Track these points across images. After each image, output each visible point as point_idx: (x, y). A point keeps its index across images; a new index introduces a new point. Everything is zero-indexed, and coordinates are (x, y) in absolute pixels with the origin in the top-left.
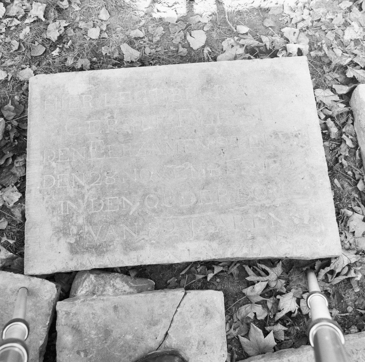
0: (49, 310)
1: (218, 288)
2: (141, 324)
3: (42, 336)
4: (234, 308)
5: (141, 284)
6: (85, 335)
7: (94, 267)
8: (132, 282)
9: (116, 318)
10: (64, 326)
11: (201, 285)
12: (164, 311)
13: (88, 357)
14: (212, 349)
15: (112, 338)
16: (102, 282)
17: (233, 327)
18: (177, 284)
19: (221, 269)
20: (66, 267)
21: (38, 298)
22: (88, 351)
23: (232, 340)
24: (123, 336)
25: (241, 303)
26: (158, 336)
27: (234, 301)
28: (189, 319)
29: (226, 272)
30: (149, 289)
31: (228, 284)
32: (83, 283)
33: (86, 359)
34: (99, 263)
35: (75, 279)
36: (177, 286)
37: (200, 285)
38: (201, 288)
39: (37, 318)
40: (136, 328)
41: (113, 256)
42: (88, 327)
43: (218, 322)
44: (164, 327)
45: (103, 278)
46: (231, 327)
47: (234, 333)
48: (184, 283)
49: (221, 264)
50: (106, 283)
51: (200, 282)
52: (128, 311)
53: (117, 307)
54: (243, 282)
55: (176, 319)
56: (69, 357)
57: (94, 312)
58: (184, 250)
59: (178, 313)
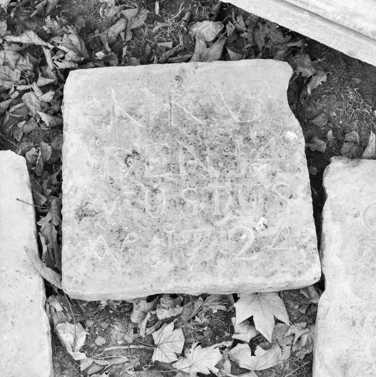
4: (287, 368)
43: (329, 350)
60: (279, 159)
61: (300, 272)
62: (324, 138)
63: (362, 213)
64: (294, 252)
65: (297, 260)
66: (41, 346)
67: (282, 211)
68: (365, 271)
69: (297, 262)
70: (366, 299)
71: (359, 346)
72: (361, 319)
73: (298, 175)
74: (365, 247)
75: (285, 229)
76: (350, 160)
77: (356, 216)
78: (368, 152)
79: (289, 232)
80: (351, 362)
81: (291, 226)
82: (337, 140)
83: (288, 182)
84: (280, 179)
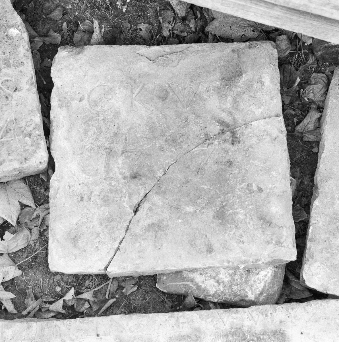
0: (310, 247)
1: (59, 277)
2: (172, 226)
3: (317, 212)
4: (37, 247)
5: (176, 285)
6: (253, 213)
7: (246, 310)
8: (190, 288)
9: (209, 236)
10: (283, 225)
11: (85, 282)
12: (138, 244)
13: (246, 184)
14: (71, 190)
15: (214, 208)
16: (235, 288)
17: (40, 220)
18: (123, 284)
19: (52, 307)
20: (290, 310)
21: (329, 264)
22: (247, 191)
23: (44, 202)
24: (198, 211)
25: (26, 254)
26: (148, 210)
27: (36, 257)
28: (103, 232)
29: (45, 302)
30: (165, 278)
31: (43, 283)
32: (265, 286)
33: (250, 181)
34: (238, 315)
35: (279, 292)
36: (122, 281)
37: (87, 282)
38: (86, 277)
39: (327, 236)
40: (180, 221)
41: (217, 328)
42: (249, 223)
43: (61, 226)
44: (139, 221)
45: (234, 294)
46: (43, 219)
47: (39, 211)
48: (112, 285)
49: (53, 314)
50: (231, 287)
51: (87, 287)
52: (192, 245)
53: (207, 251)
54: (19, 285)
55: (121, 232)
56: (272, 184)
57: (242, 245)
58: (105, 335)
59: (119, 241)
60: (3, 55)
61: (26, 159)
62: (60, 31)
63: (86, 96)
64: (20, 141)
65: (23, 148)
66: (295, 254)
67: (8, 104)
68: (91, 150)
69: (22, 150)
70: (93, 175)
71: (87, 219)
72: (88, 194)
73: (21, 68)
74: (90, 128)
75: (11, 121)
76: (74, 48)
77: (81, 100)
78: (94, 38)
79: (15, 123)
80: (81, 234)
81: (17, 117)
82: (72, 31)
83: (12, 77)
84: (6, 75)
